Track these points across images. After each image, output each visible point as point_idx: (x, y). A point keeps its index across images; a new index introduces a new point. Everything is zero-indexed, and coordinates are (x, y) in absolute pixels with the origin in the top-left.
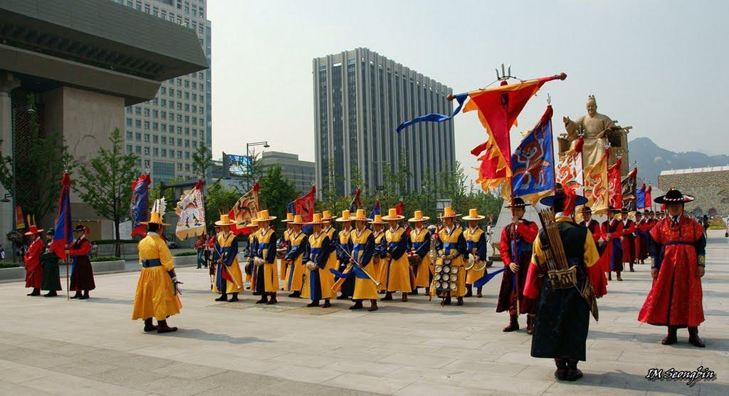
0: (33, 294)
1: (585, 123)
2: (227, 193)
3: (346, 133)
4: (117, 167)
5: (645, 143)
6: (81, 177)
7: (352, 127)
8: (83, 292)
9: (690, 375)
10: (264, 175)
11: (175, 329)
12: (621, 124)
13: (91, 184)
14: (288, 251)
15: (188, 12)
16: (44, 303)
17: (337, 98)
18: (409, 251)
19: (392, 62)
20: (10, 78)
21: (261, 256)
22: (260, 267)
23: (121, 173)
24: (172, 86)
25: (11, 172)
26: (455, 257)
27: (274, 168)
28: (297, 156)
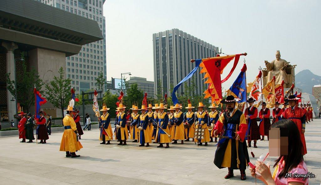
0: (22, 142)
1: (275, 63)
2: (113, 96)
3: (168, 68)
4: (62, 85)
5: (307, 73)
6: (46, 90)
7: (171, 65)
8: (43, 141)
9: (304, 176)
10: (129, 88)
11: (79, 156)
12: (292, 64)
13: (50, 93)
14: (132, 122)
15: (94, 13)
16: (27, 146)
17: (164, 52)
18: (185, 122)
19: (189, 35)
20: (13, 45)
21: (119, 124)
22: (119, 129)
23: (64, 88)
24: (88, 47)
25: (15, 88)
26: (203, 124)
27: (134, 84)
28: (146, 79)
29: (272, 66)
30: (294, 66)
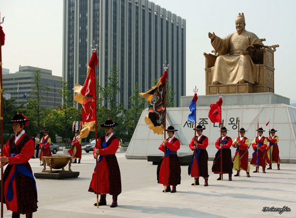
1: (233, 40)
9: (280, 209)
14: (76, 137)
17: (83, 22)
28: (51, 71)
29: (227, 46)
30: (272, 47)
